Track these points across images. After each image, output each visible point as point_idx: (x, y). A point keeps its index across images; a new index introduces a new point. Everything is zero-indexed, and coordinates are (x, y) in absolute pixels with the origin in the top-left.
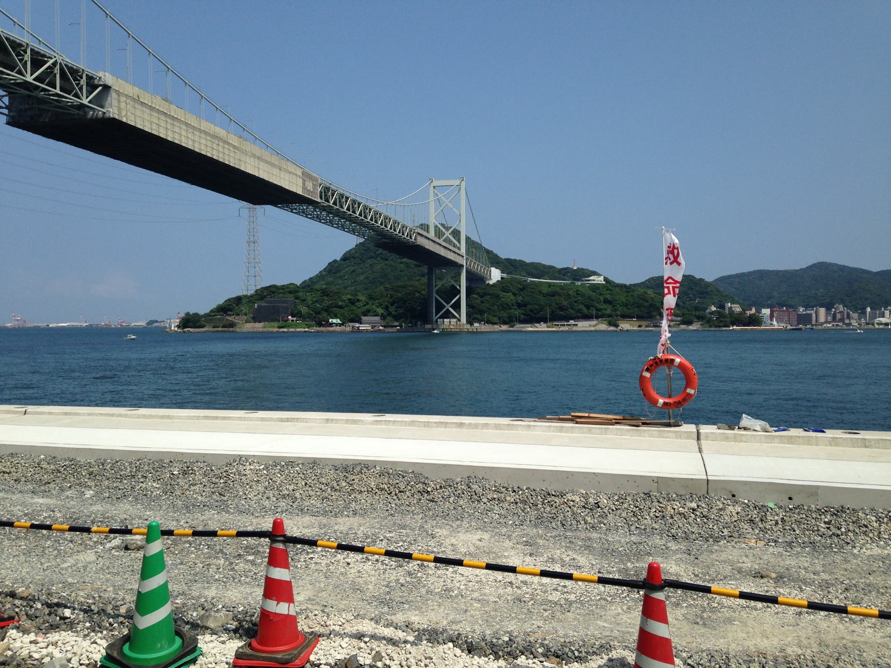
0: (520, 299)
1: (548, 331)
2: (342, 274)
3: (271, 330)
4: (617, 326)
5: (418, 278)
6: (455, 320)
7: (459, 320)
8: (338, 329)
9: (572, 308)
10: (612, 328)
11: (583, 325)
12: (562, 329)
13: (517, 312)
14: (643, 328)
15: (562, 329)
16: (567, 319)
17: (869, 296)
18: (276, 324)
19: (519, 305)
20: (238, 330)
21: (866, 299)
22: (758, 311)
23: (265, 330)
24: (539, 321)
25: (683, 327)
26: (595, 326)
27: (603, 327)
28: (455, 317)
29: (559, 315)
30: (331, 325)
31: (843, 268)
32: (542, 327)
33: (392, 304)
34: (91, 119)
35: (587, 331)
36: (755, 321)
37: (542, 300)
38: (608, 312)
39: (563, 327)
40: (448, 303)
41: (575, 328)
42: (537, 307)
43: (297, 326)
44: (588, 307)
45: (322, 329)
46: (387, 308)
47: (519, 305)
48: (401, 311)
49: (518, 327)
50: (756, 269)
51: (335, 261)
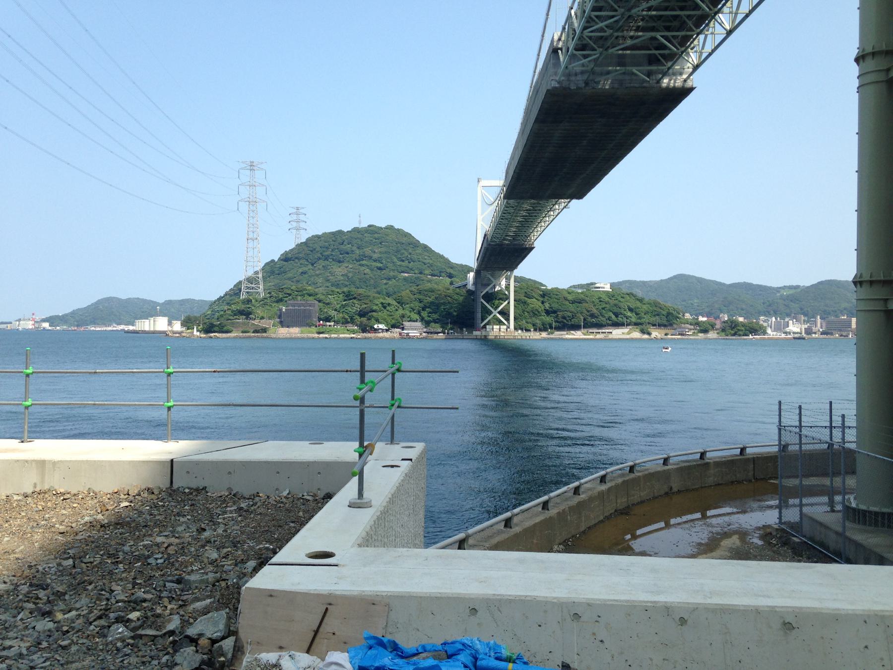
0: (547, 305)
1: (585, 339)
2: (290, 275)
3: (311, 335)
4: (649, 334)
5: (385, 281)
6: (505, 327)
7: (508, 327)
8: (387, 335)
9: (603, 316)
10: (646, 336)
11: (617, 333)
12: (598, 336)
13: (548, 319)
14: (669, 336)
15: (598, 336)
16: (599, 326)
17: (744, 307)
18: (314, 329)
19: (548, 312)
20: (273, 336)
21: (742, 309)
22: (757, 319)
23: (305, 335)
24: (576, 327)
25: (701, 335)
26: (629, 333)
27: (636, 335)
28: (504, 324)
29: (593, 323)
30: (376, 331)
31: (700, 280)
32: (578, 334)
33: (424, 309)
34: (667, 88)
35: (623, 339)
36: (754, 330)
37: (572, 308)
38: (634, 320)
39: (598, 335)
40: (491, 313)
41: (610, 336)
42: (570, 314)
43: (337, 332)
44: (616, 315)
45: (369, 335)
46: (419, 313)
47: (548, 312)
48: (435, 316)
49: (557, 334)
50: (788, 283)
51: (273, 261)
